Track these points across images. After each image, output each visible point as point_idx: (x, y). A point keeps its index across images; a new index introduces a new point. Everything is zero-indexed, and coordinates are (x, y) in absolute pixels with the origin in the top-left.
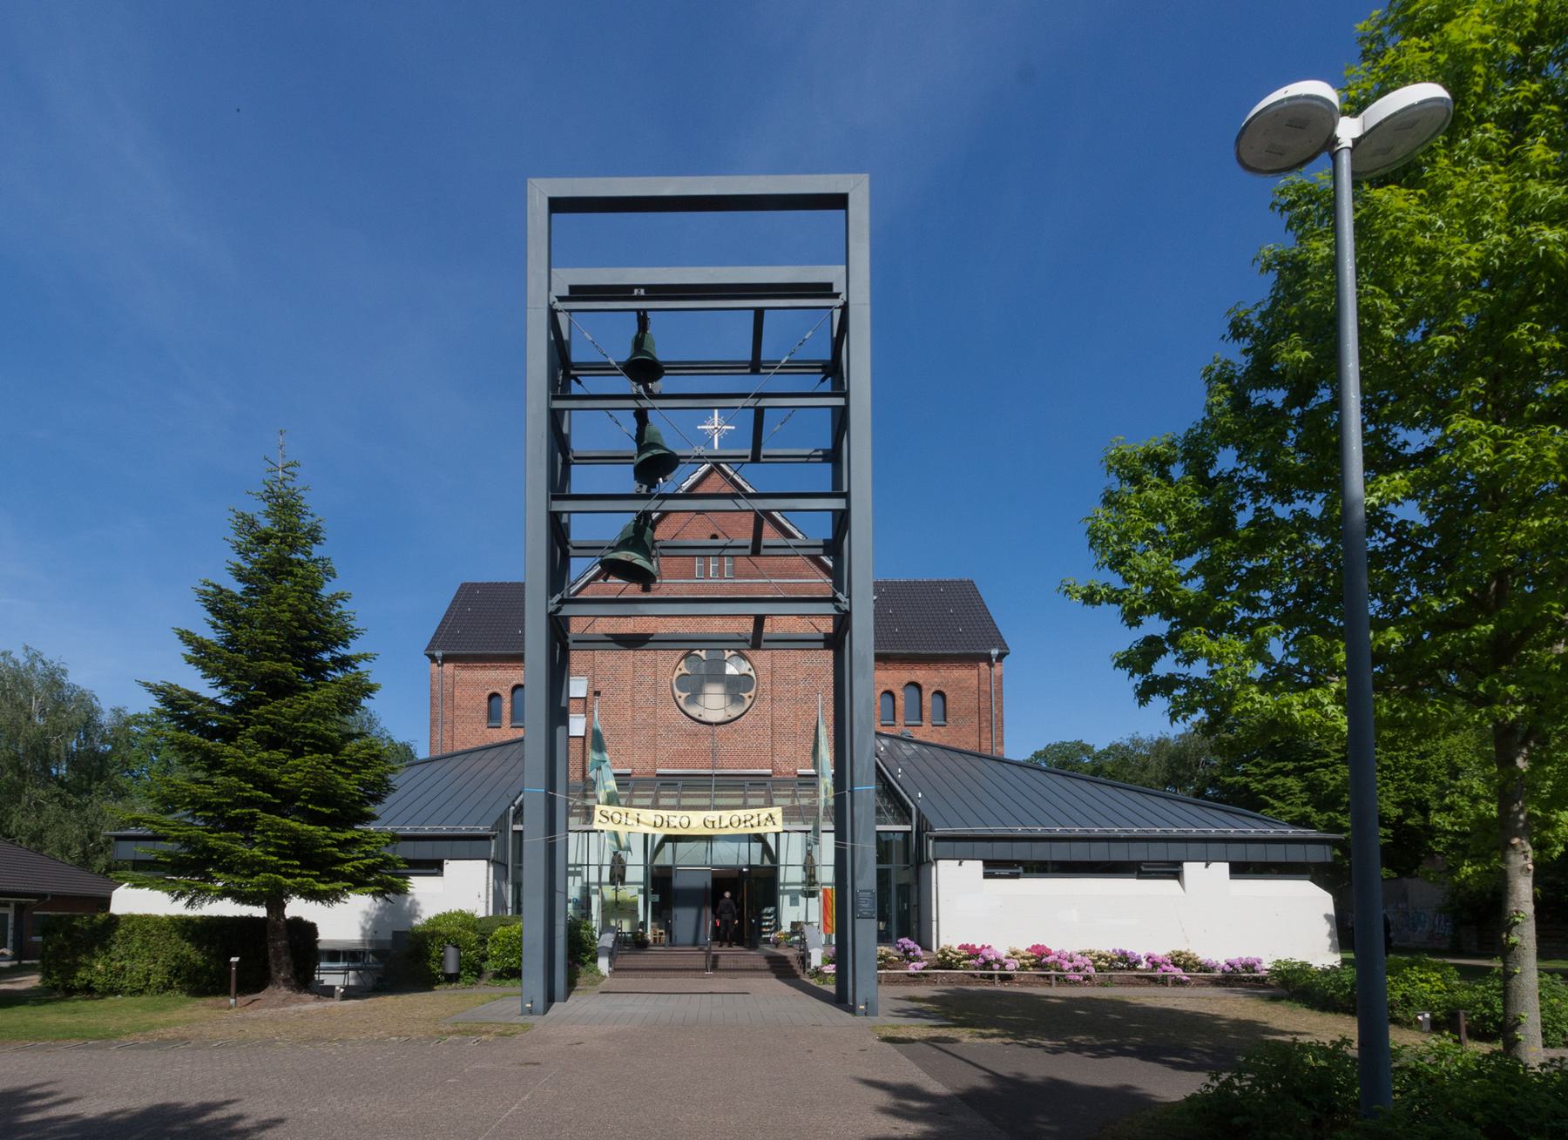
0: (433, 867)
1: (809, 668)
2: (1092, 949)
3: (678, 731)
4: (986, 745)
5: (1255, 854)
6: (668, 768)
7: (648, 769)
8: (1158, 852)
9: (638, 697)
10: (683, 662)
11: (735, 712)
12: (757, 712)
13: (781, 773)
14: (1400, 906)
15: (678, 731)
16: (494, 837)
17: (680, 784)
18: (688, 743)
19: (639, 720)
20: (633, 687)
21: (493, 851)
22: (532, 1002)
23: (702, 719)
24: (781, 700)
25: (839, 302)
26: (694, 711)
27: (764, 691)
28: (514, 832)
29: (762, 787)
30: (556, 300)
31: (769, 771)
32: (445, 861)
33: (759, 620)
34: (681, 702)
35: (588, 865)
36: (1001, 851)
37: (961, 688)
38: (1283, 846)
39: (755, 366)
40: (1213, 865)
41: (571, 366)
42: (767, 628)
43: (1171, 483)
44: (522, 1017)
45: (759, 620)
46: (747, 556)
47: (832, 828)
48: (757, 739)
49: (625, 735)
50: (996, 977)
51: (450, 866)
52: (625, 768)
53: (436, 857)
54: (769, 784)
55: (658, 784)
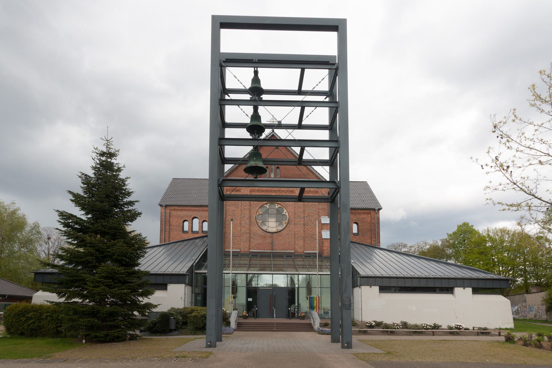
0: (163, 287)
1: (308, 212)
2: (439, 323)
3: (258, 235)
4: (373, 243)
5: (481, 285)
6: (259, 250)
7: (246, 250)
8: (445, 284)
9: (242, 222)
10: (260, 209)
11: (280, 228)
12: (288, 229)
13: (298, 252)
14: (523, 304)
15: (258, 235)
16: (188, 275)
17: (259, 256)
18: (262, 240)
19: (243, 231)
20: (241, 218)
21: (187, 281)
22: (210, 342)
23: (267, 231)
24: (298, 224)
25: (335, 67)
26: (264, 228)
27: (291, 221)
28: (195, 273)
29: (291, 258)
30: (222, 62)
31: (293, 251)
32: (168, 284)
33: (302, 190)
34: (259, 224)
35: (321, 288)
36: (386, 283)
37: (364, 222)
38: (156, 283)
39: (300, 92)
40: (466, 289)
41: (226, 91)
42: (305, 194)
43: (9, 231)
44: (207, 349)
45: (302, 190)
46: (296, 165)
47: (329, 273)
48: (288, 239)
49: (237, 236)
50: (389, 332)
51: (457, 290)
52: (237, 249)
53: (451, 286)
54: (293, 256)
55: (250, 256)
